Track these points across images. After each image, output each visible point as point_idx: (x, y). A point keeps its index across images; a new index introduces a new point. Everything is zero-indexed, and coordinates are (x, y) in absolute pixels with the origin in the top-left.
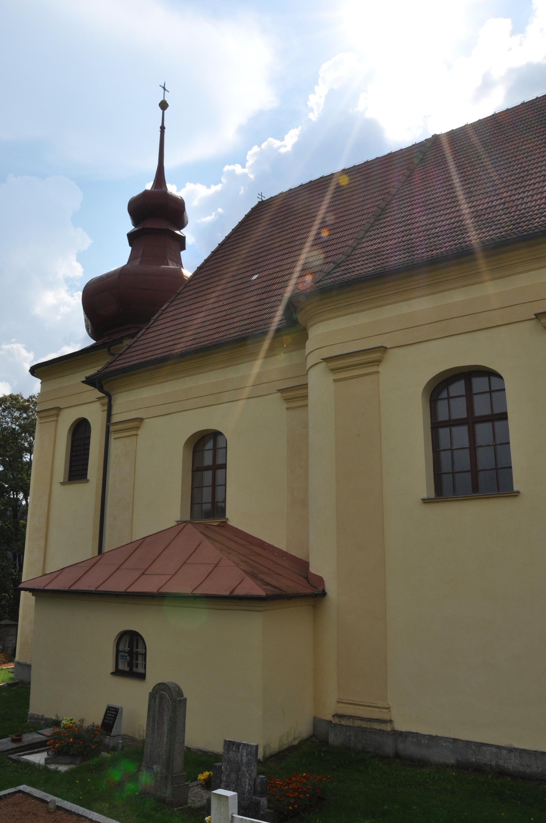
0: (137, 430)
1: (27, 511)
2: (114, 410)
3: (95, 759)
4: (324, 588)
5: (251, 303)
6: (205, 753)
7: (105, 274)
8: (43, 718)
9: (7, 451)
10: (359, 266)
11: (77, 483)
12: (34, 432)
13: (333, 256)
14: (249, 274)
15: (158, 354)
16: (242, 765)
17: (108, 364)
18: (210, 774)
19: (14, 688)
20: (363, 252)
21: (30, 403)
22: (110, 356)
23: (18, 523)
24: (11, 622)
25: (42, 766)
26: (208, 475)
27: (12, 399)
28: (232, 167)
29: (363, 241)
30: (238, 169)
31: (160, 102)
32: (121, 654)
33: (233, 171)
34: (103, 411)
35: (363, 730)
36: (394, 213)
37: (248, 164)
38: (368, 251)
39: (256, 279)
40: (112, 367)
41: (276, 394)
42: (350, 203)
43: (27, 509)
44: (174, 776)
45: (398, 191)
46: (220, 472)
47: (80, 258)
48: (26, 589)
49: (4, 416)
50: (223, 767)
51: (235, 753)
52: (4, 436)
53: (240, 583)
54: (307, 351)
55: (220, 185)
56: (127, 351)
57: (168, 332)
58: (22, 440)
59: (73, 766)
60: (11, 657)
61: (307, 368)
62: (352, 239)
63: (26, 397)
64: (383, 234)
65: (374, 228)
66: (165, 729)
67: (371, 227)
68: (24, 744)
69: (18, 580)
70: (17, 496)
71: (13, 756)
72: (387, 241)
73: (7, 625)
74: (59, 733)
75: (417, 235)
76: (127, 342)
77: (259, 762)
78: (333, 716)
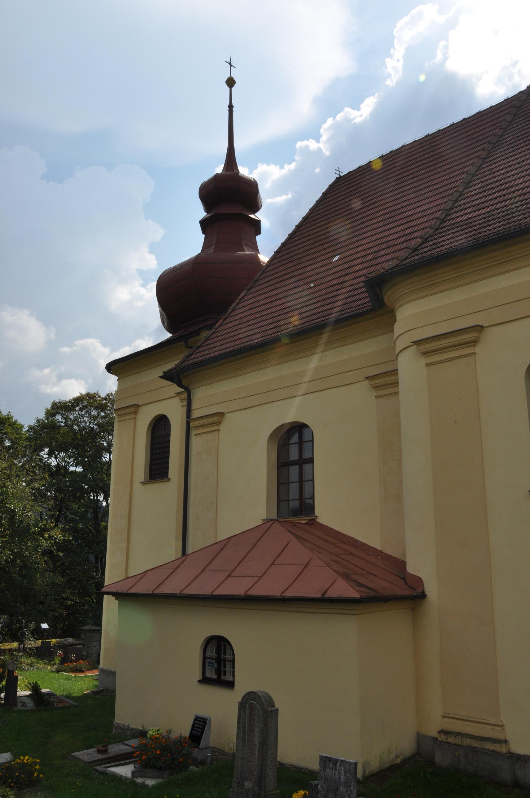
0: (219, 425)
1: (108, 512)
2: (194, 406)
3: (184, 772)
4: (423, 590)
5: (333, 286)
6: (299, 770)
7: (179, 264)
8: (128, 728)
9: (86, 451)
10: (449, 239)
11: (158, 482)
12: (112, 431)
13: (420, 230)
14: (329, 255)
15: (238, 345)
16: (340, 784)
17: (186, 358)
18: (305, 793)
19: (99, 696)
20: (452, 224)
21: (107, 402)
22: (187, 349)
23: (99, 525)
24: (94, 628)
25: (129, 779)
26: (294, 470)
27: (89, 398)
28: (305, 143)
29: (452, 212)
30: (313, 145)
31: (226, 79)
32: (208, 660)
33: (307, 147)
34: (182, 406)
35: (474, 750)
36: (486, 179)
37: (324, 138)
38: (458, 223)
39: (337, 261)
40: (190, 360)
41: (363, 383)
42: (436, 171)
43: (108, 510)
44: (267, 794)
45: (489, 154)
46: (307, 467)
47: (153, 249)
48: (108, 593)
49: (82, 415)
50: (319, 786)
51: (332, 770)
52: (82, 435)
53: (332, 585)
54: (396, 334)
55: (294, 163)
56: (205, 344)
57: (247, 322)
58: (101, 439)
59: (160, 780)
60: (95, 664)
61: (397, 352)
62: (439, 211)
63: (103, 395)
64: (474, 203)
65: (464, 197)
66: (257, 741)
67: (460, 196)
68: (110, 756)
69: (100, 584)
70: (97, 498)
71: (99, 768)
72: (479, 210)
73: (90, 631)
74: (145, 745)
75: (512, 200)
76: (205, 334)
77: (358, 781)
78: (439, 732)
